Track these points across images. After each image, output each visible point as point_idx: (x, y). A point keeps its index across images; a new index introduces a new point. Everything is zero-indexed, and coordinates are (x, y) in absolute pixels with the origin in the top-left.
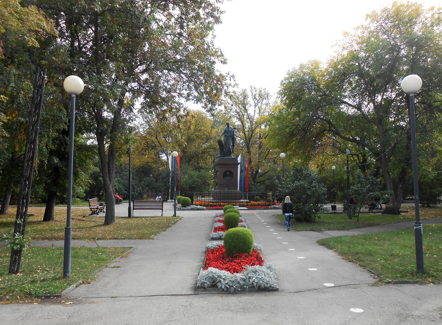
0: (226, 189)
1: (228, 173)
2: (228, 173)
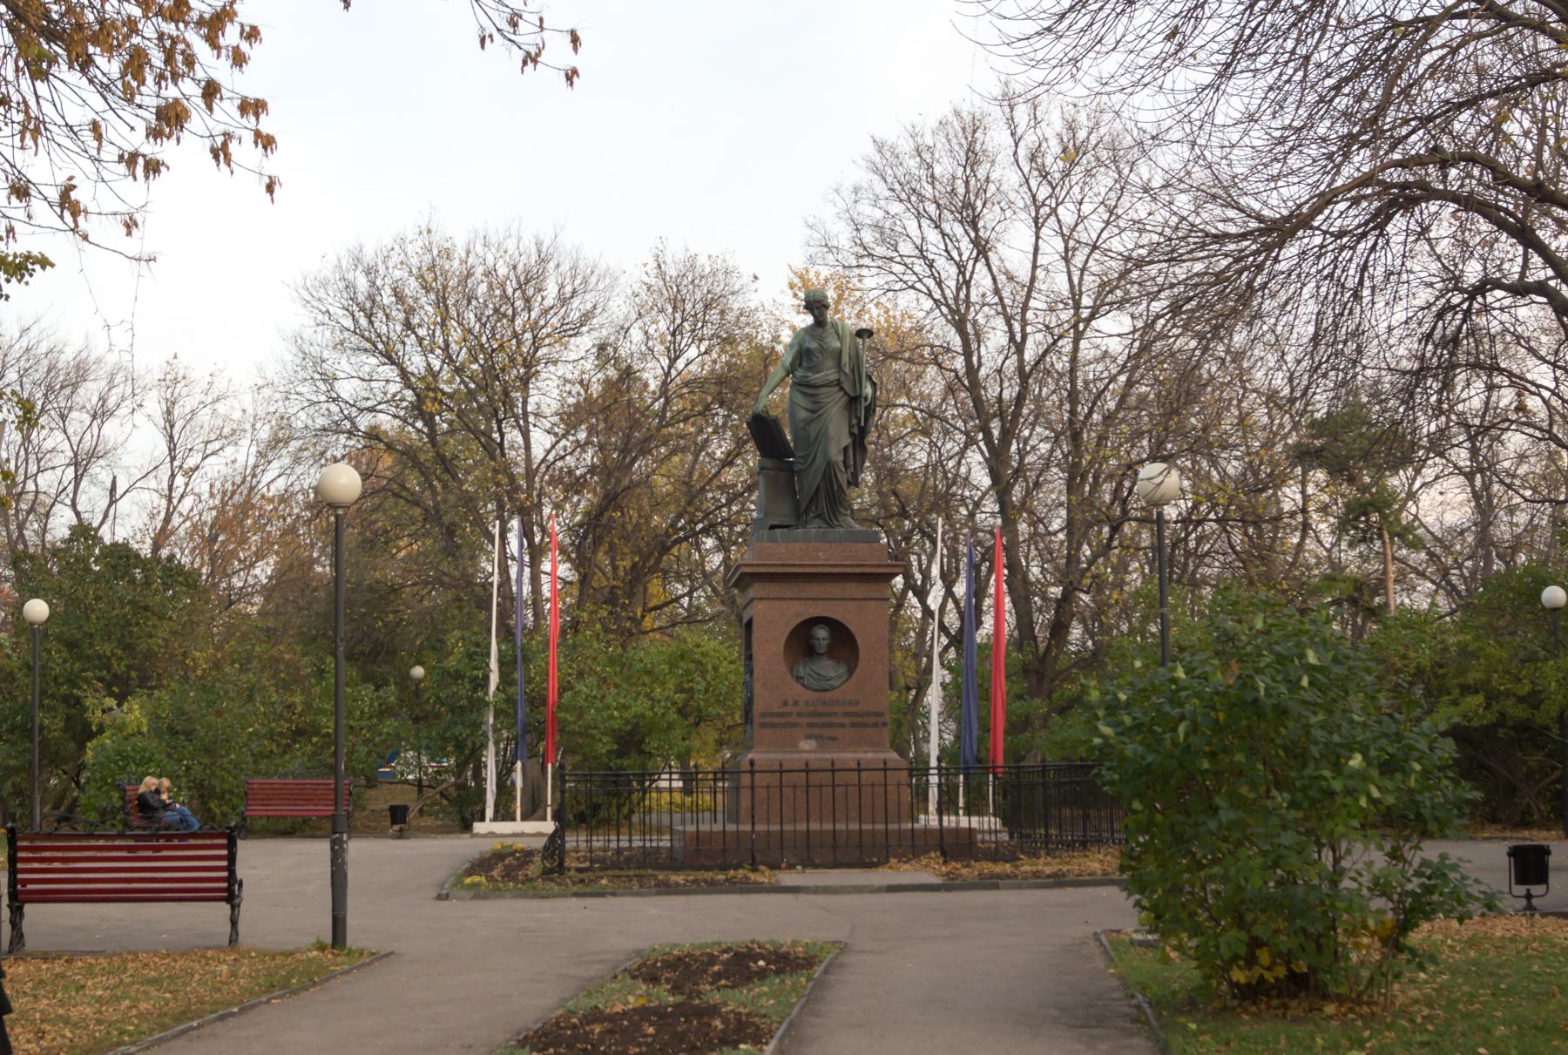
0: (807, 745)
1: (822, 633)
2: (822, 633)
